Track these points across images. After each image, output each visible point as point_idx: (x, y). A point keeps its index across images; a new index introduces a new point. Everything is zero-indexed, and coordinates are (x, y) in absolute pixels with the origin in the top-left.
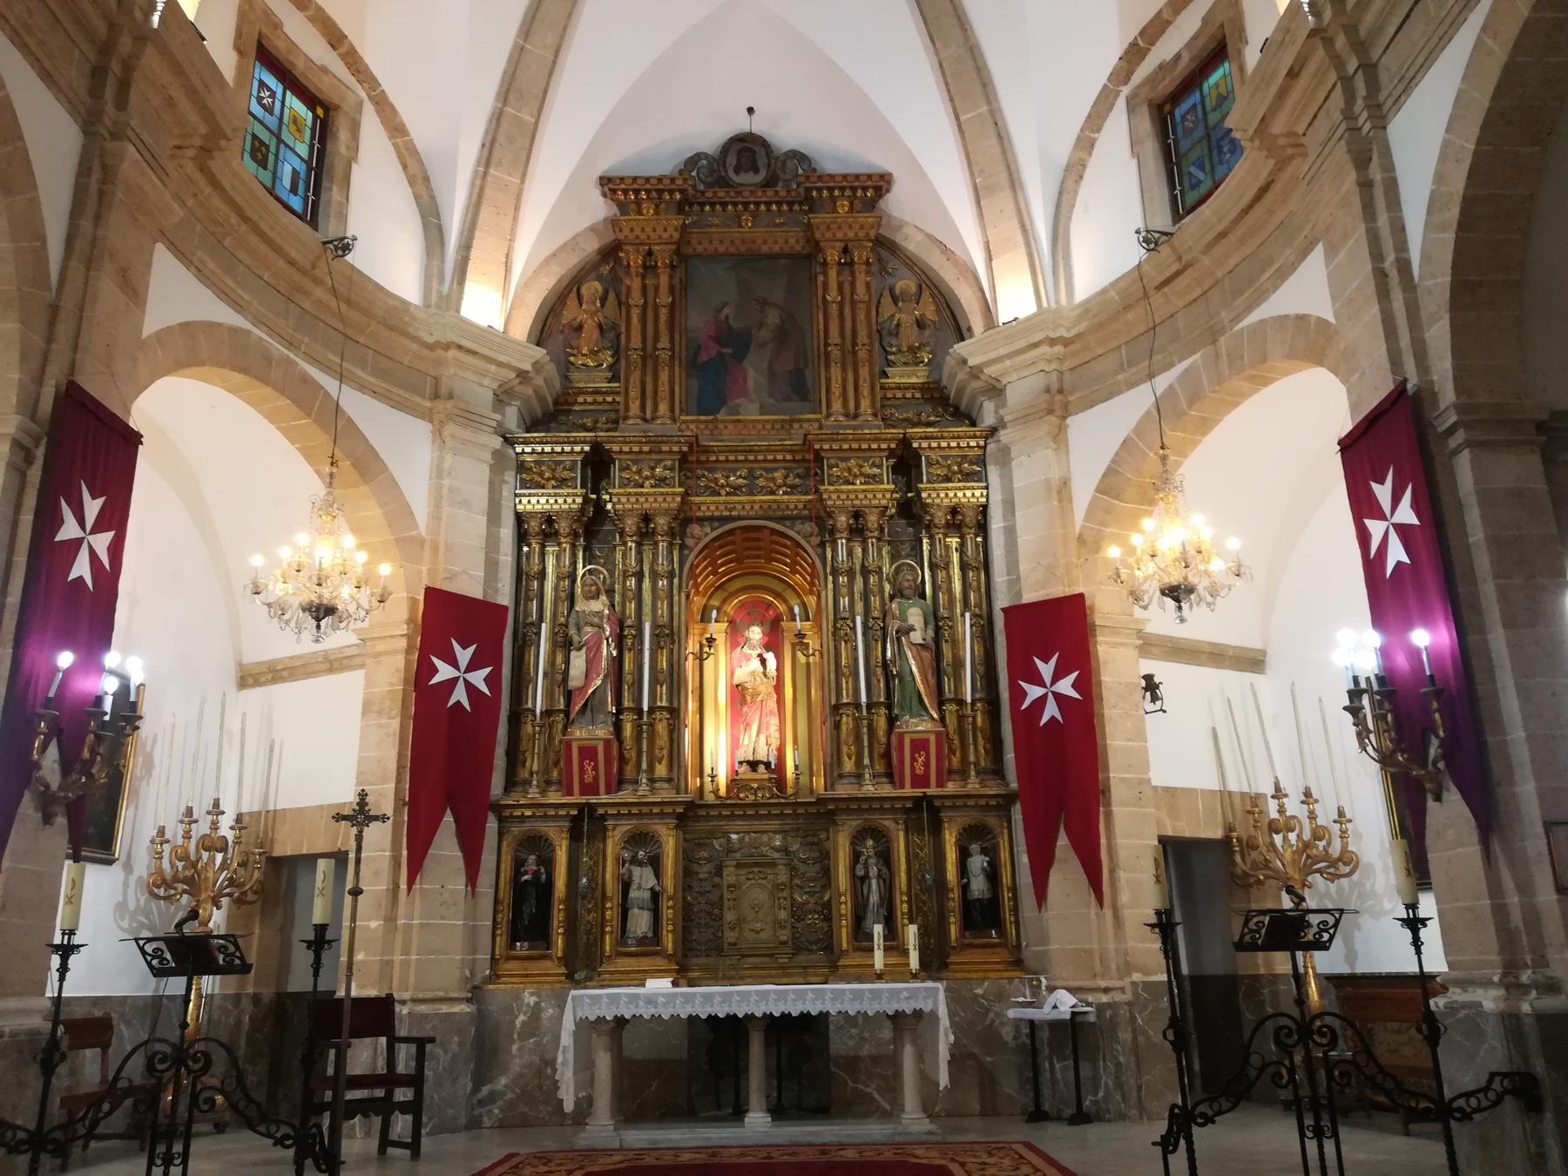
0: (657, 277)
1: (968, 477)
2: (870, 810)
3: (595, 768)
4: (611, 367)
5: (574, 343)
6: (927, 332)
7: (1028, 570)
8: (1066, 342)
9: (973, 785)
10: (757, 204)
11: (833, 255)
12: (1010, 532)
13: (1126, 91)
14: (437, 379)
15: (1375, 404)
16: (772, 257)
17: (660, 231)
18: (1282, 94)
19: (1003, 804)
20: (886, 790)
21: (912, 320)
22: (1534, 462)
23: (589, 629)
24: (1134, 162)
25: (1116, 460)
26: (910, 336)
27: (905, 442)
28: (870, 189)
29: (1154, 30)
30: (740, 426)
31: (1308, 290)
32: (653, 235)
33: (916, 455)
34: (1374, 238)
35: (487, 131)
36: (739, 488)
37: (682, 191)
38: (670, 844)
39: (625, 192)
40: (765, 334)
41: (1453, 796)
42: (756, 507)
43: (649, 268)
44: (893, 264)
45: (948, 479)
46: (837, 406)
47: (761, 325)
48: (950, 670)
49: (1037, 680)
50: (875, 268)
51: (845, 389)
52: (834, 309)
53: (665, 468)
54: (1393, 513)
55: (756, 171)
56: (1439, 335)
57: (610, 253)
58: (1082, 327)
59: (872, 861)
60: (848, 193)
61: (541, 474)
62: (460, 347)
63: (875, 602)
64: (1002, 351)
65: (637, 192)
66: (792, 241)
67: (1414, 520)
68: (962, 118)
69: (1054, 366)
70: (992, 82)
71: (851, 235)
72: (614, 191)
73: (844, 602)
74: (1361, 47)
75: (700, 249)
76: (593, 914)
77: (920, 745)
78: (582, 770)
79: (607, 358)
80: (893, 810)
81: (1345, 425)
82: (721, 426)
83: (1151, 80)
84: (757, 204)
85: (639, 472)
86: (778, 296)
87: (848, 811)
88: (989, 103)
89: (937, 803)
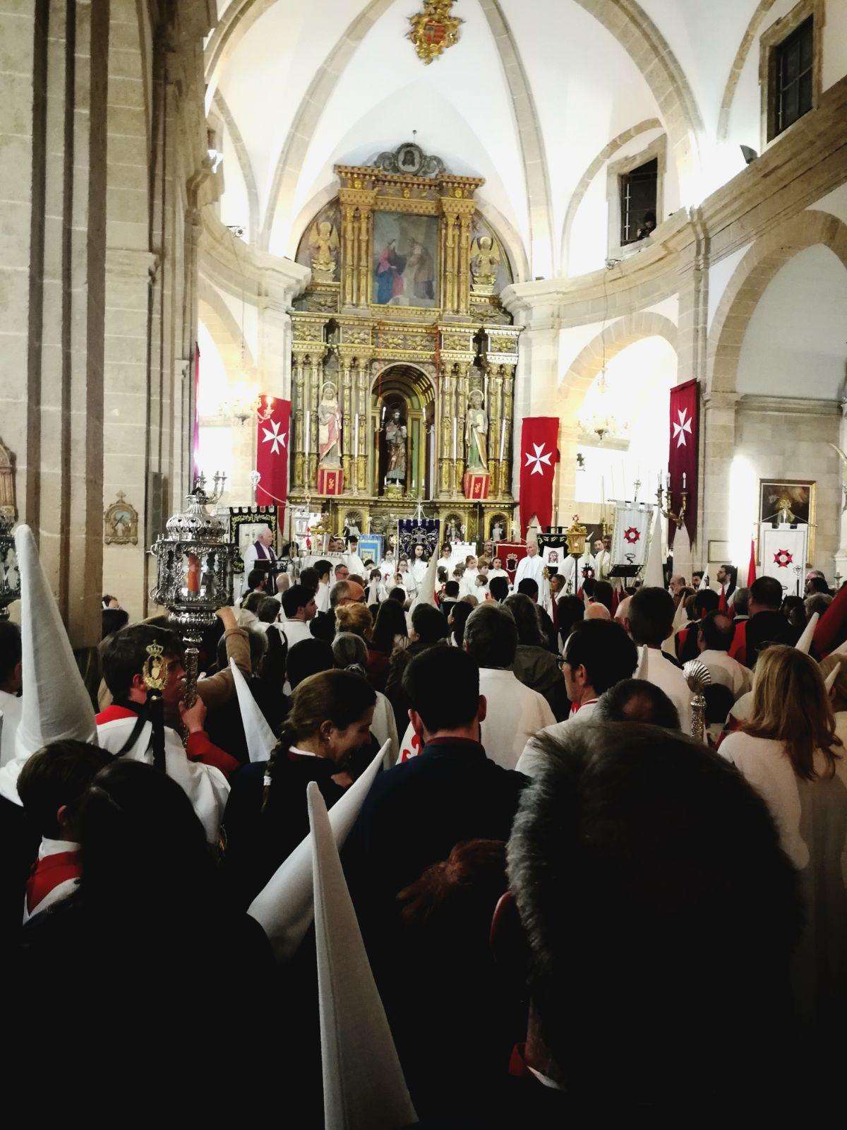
0: (360, 223)
1: (510, 350)
2: (455, 507)
3: (334, 483)
4: (334, 272)
5: (316, 256)
6: (494, 266)
7: (533, 401)
8: (564, 293)
9: (499, 499)
10: (413, 184)
11: (451, 221)
12: (527, 381)
13: (608, 162)
14: (259, 284)
15: (685, 381)
16: (419, 215)
17: (363, 198)
18: (674, 236)
19: (513, 505)
20: (462, 499)
21: (488, 259)
22: (732, 415)
23: (328, 415)
24: (607, 204)
25: (580, 356)
26: (486, 269)
27: (482, 330)
28: (470, 185)
29: (625, 137)
30: (400, 311)
31: (670, 308)
32: (360, 201)
33: (486, 336)
34: (697, 314)
35: (285, 144)
36: (398, 345)
37: (376, 176)
38: (367, 519)
39: (346, 173)
40: (413, 259)
41: (684, 528)
42: (407, 356)
43: (356, 218)
44: (480, 225)
45: (500, 350)
46: (449, 305)
47: (411, 254)
48: (493, 445)
49: (534, 454)
50: (470, 229)
51: (453, 296)
52: (450, 251)
53: (365, 334)
54: (684, 424)
55: (413, 165)
56: (711, 361)
57: (335, 203)
58: (573, 288)
59: (453, 529)
60: (461, 185)
61: (304, 333)
62: (274, 270)
63: (461, 410)
64: (534, 293)
65: (352, 174)
66: (430, 208)
67: (690, 431)
68: (527, 163)
69: (556, 303)
70: (543, 139)
71: (461, 210)
72: (340, 172)
73: (447, 409)
74: (705, 231)
75: (382, 208)
76: (119, 517)
77: (479, 480)
78: (328, 484)
79: (332, 266)
80: (464, 508)
81: (675, 385)
82: (391, 310)
83: (619, 163)
84: (413, 184)
85: (352, 335)
86: (420, 238)
87: (445, 507)
88: (541, 158)
89: (483, 506)
